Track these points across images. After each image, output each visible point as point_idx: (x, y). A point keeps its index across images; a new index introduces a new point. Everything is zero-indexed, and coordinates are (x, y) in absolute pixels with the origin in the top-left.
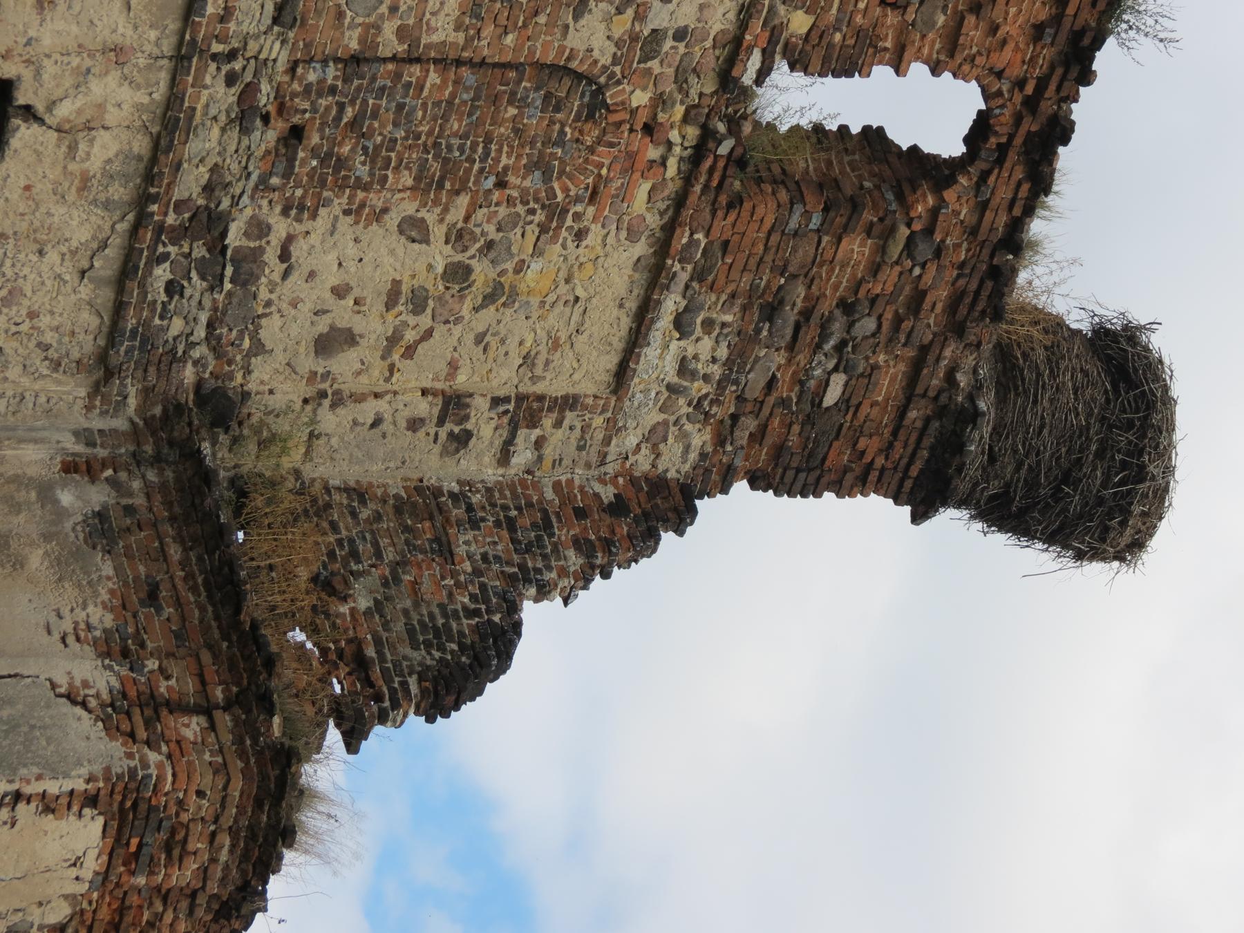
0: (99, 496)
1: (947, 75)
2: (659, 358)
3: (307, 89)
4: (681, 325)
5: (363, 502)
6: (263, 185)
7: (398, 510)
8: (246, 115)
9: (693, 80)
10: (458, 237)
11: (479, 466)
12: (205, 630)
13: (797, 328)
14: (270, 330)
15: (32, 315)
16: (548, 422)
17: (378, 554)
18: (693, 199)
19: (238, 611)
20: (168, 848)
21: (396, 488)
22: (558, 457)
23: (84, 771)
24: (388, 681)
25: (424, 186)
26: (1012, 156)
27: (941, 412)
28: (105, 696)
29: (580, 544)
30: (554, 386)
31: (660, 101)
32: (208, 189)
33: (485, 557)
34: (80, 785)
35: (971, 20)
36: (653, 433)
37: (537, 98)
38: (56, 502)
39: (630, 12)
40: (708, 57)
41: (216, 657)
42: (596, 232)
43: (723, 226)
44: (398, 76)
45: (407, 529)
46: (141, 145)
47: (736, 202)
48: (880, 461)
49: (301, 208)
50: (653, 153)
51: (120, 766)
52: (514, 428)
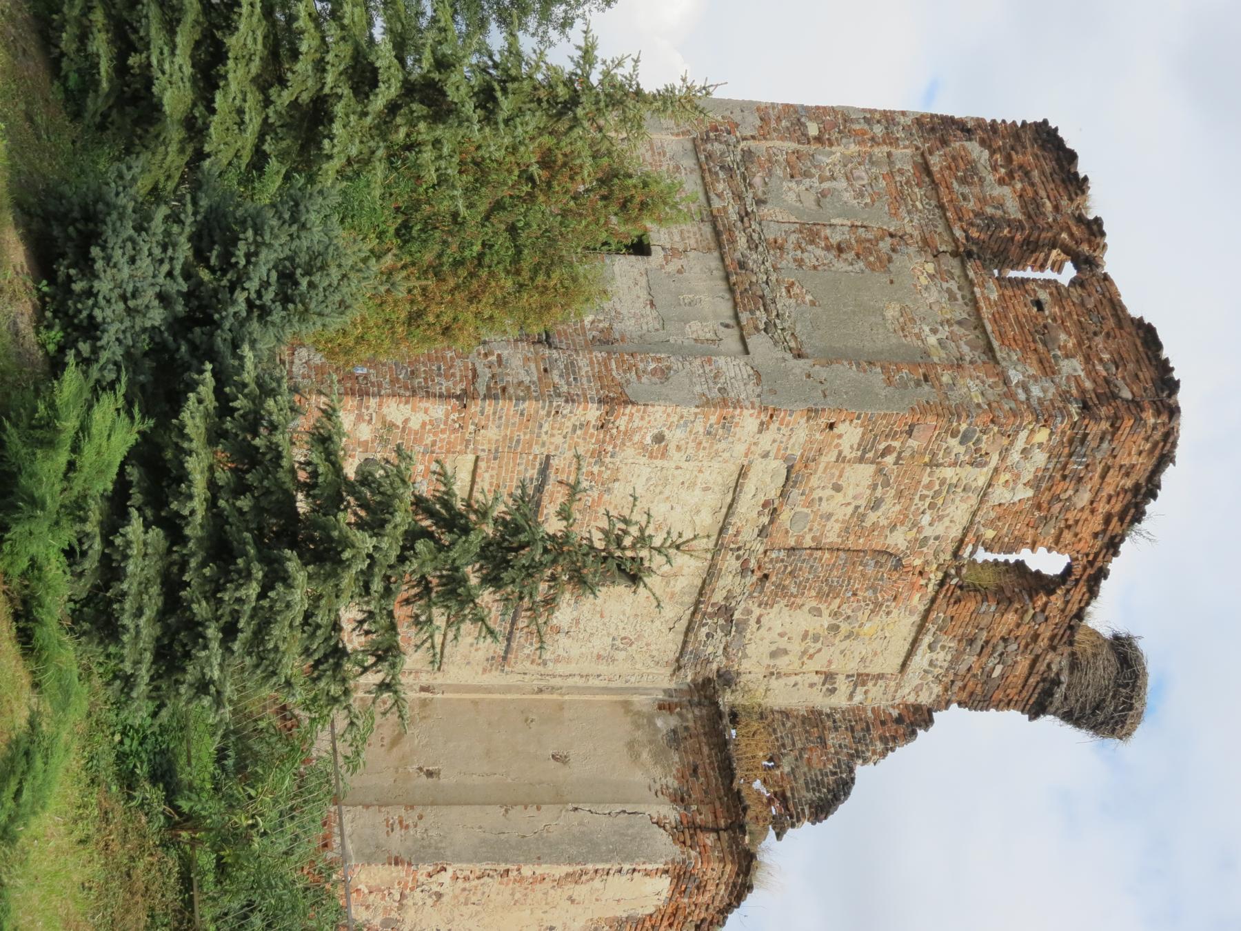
0: (673, 721)
1: (1054, 553)
2: (921, 659)
3: (771, 561)
4: (931, 647)
5: (788, 718)
6: (751, 596)
7: (803, 723)
8: (744, 570)
9: (941, 554)
10: (835, 614)
11: (840, 700)
12: (718, 790)
13: (982, 647)
14: (751, 649)
15: (647, 645)
16: (870, 684)
17: (794, 744)
18: (938, 601)
19: (732, 782)
20: (698, 888)
21: (803, 712)
22: (877, 698)
23: (663, 860)
24: (796, 808)
25: (821, 596)
26: (1082, 583)
27: (1044, 680)
28: (673, 824)
29: (883, 739)
30: (874, 669)
31: (927, 563)
32: (726, 598)
33: (840, 746)
34: (661, 866)
35: (1066, 532)
36: (917, 688)
37: (872, 563)
38: (655, 725)
39: (915, 530)
40: (950, 548)
41: (722, 804)
42: (895, 613)
43: (952, 610)
44: (811, 555)
45: (807, 732)
46: (699, 582)
47: (958, 601)
48: (1016, 698)
49: (766, 604)
50: (923, 582)
51: (679, 858)
52: (855, 686)
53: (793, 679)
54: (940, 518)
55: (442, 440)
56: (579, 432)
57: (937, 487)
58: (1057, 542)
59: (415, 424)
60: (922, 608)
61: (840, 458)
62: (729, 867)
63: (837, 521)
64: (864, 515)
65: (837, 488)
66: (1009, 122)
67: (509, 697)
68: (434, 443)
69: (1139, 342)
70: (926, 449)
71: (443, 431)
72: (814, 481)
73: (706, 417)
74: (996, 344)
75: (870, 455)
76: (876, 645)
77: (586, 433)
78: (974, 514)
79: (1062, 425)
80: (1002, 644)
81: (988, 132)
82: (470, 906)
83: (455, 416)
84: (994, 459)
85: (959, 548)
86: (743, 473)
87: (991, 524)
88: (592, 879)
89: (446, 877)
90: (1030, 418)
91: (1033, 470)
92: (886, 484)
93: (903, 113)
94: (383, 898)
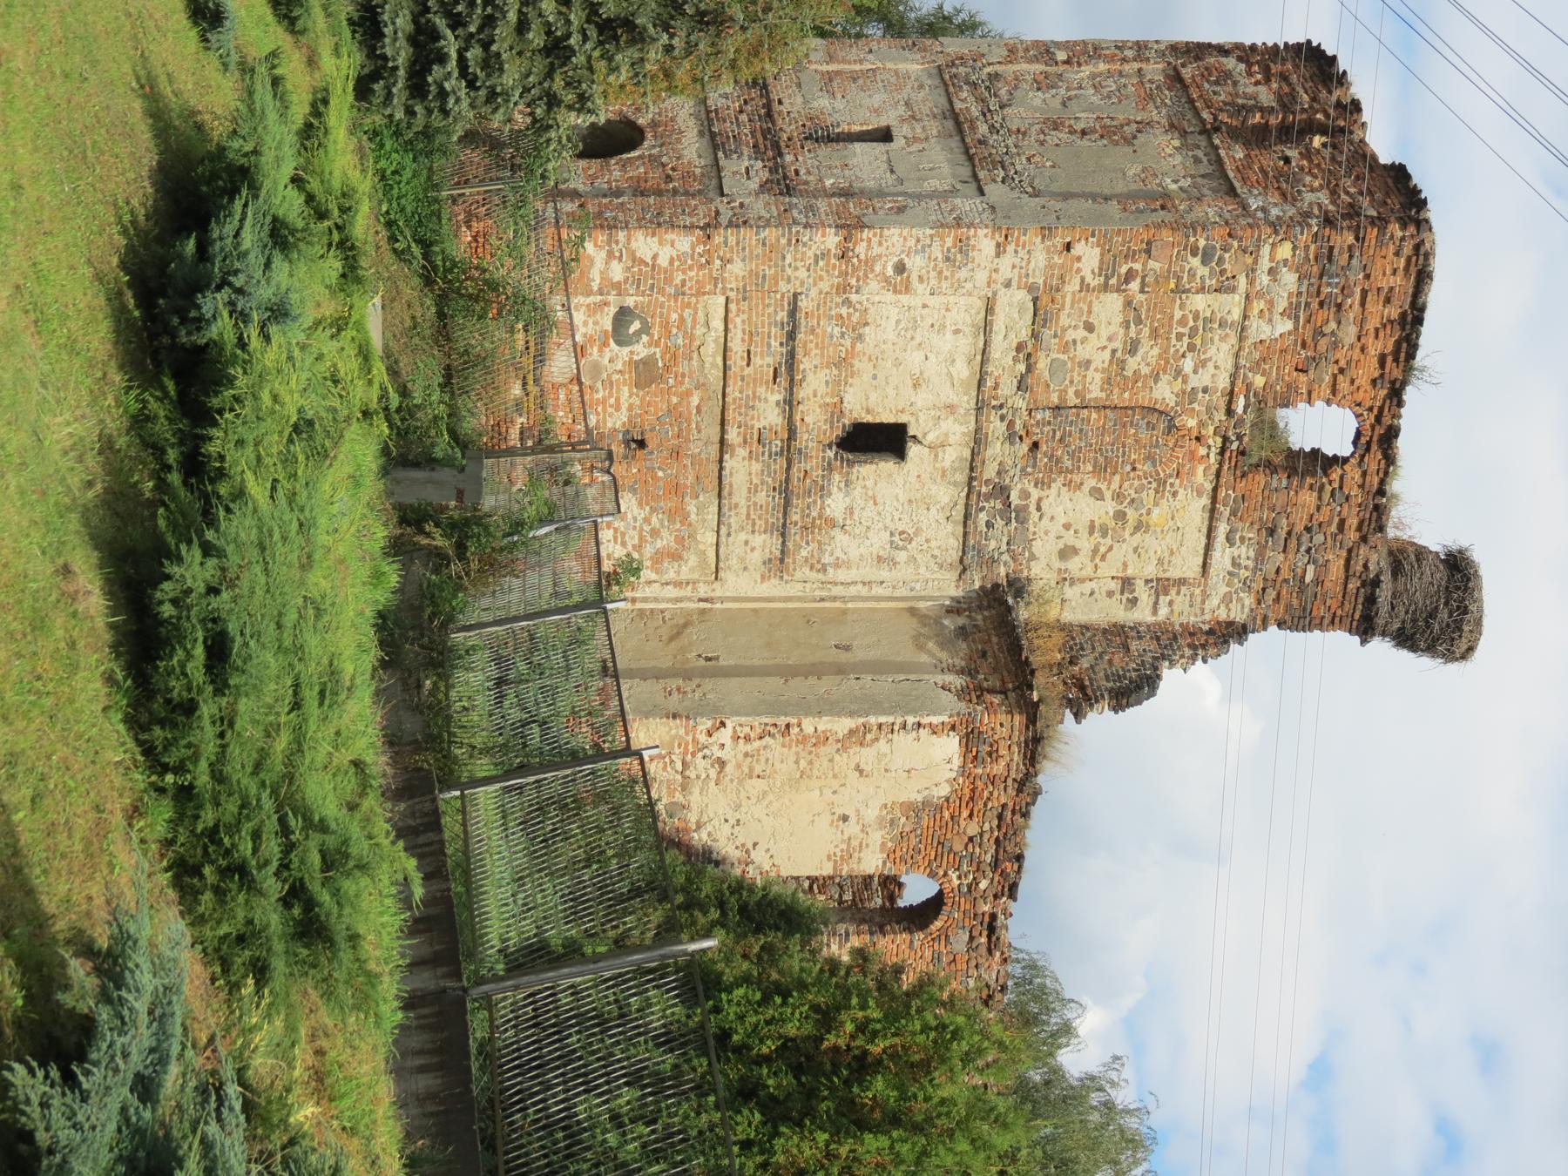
0: (961, 621)
2: (1222, 556)
8: (1011, 436)
11: (1142, 614)
14: (1037, 546)
16: (1173, 592)
22: (1180, 610)
25: (1101, 470)
30: (1174, 573)
31: (1201, 424)
32: (999, 473)
34: (946, 719)
35: (1340, 378)
36: (1222, 600)
46: (967, 453)
53: (1088, 586)
54: (1204, 363)
55: (691, 279)
56: (821, 263)
57: (1191, 323)
58: (1334, 392)
59: (663, 261)
60: (1209, 487)
61: (1084, 287)
62: (1017, 718)
63: (1096, 370)
64: (1123, 361)
65: (1090, 328)
66: (1270, 44)
67: (790, 605)
68: (684, 282)
69: (1390, 181)
70: (1169, 271)
71: (691, 268)
72: (1064, 320)
73: (942, 239)
74: (1237, 185)
75: (1113, 281)
76: (1170, 539)
77: (827, 265)
78: (1237, 356)
79: (1304, 238)
80: (1306, 537)
81: (1246, 53)
82: (755, 780)
83: (700, 249)
84: (1242, 281)
85: (1230, 403)
86: (989, 310)
87: (1256, 367)
88: (877, 739)
89: (725, 735)
90: (1269, 231)
91: (1285, 295)
92: (1138, 321)
93: (1157, 42)
94: (665, 769)
